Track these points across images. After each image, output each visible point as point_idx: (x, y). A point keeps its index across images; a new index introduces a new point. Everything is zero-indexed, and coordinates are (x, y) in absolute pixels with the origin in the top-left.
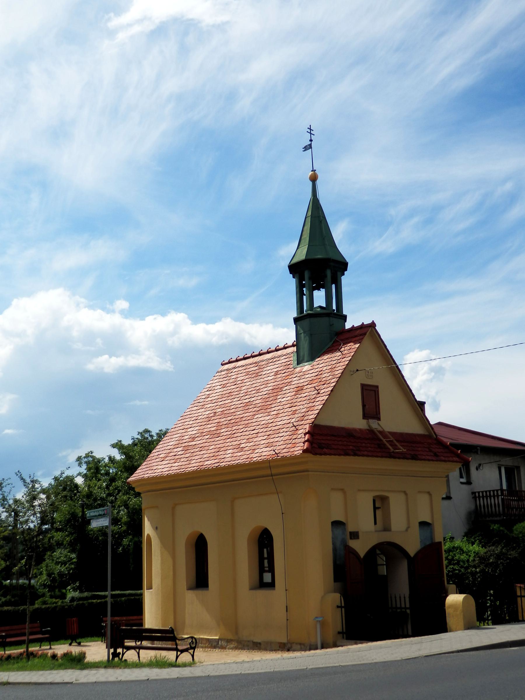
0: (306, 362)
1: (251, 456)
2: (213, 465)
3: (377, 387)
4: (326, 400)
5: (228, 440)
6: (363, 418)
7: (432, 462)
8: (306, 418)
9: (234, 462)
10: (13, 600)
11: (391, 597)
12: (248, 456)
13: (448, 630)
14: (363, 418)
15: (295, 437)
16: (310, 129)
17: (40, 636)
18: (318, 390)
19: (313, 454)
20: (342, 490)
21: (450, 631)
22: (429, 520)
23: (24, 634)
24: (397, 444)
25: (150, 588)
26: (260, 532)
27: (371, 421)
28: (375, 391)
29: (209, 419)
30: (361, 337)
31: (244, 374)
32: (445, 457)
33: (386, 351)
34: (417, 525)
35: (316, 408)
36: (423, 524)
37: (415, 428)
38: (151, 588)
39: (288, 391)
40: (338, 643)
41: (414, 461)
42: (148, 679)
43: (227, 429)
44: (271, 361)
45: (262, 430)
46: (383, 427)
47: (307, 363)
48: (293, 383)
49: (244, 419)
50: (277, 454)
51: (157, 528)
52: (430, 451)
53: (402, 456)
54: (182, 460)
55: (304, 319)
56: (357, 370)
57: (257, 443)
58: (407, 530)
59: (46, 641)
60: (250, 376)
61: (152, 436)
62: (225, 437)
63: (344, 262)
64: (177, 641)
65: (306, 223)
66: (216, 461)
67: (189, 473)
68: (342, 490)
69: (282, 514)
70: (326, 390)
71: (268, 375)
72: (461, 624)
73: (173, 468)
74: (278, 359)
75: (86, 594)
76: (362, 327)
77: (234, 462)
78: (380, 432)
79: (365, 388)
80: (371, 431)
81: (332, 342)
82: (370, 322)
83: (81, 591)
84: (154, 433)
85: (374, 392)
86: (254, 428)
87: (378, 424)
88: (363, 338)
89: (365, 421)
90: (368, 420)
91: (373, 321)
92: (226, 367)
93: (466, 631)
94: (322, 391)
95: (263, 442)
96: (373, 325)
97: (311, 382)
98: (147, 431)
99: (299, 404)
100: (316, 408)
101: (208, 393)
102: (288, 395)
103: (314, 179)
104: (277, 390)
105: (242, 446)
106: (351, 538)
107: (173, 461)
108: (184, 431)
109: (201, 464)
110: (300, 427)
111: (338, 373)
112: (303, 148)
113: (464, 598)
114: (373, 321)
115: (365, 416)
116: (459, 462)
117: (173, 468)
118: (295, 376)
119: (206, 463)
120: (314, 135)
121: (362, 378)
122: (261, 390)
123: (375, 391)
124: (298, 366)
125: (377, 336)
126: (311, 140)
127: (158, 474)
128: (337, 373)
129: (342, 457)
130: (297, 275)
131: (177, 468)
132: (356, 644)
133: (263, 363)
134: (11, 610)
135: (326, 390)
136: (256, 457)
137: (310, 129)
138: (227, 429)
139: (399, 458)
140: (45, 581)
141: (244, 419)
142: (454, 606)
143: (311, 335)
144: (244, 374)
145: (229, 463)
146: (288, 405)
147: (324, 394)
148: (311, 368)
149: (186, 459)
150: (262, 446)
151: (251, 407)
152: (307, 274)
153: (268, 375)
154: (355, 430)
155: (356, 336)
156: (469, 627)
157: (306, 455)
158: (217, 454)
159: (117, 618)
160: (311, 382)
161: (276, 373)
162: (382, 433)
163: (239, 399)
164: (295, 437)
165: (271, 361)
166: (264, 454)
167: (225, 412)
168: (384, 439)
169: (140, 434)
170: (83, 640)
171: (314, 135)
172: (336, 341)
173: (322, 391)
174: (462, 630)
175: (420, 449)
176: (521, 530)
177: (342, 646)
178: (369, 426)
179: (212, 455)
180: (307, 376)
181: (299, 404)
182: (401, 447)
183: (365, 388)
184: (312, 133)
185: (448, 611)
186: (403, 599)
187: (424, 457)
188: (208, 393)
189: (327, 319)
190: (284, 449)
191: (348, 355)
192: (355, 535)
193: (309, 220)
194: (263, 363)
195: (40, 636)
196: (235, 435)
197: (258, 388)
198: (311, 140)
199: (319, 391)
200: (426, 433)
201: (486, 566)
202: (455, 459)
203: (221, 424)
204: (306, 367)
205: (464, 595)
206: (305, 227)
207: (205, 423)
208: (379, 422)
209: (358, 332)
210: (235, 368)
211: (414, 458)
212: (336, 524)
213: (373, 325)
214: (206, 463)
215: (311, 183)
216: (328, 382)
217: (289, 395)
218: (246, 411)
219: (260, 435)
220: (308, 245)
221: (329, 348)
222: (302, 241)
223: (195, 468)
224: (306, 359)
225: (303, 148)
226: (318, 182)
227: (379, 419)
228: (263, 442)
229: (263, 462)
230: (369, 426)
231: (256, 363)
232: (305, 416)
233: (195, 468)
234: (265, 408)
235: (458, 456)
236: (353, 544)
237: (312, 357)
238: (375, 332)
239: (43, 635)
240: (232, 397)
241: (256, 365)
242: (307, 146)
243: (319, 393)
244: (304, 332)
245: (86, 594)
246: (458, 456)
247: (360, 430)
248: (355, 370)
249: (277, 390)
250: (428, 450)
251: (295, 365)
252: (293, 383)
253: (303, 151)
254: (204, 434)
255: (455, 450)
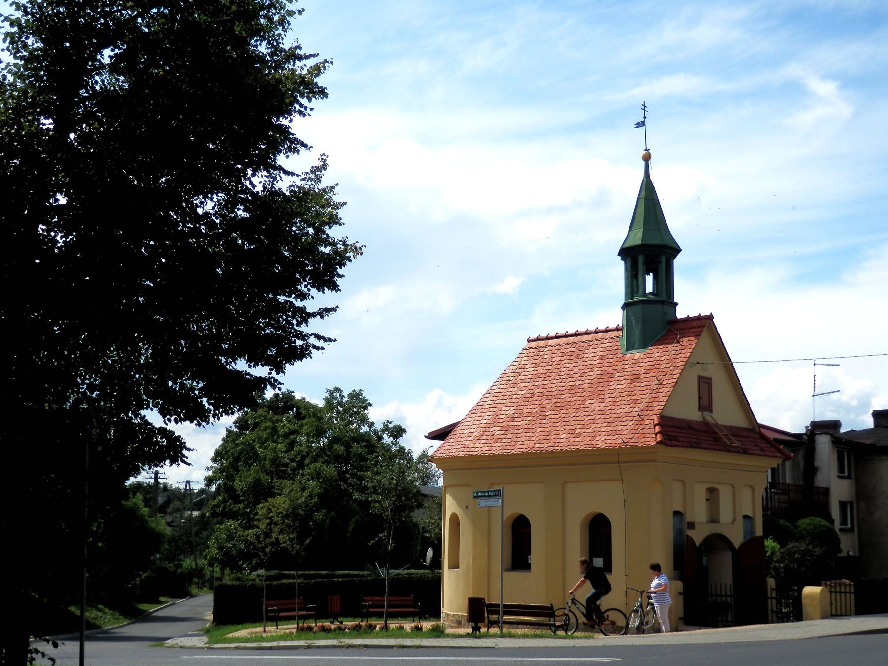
0: (638, 349)
1: (593, 442)
2: (547, 449)
3: (711, 379)
4: (671, 392)
5: (559, 424)
6: (699, 411)
7: (760, 457)
8: (651, 408)
9: (573, 447)
10: (153, 575)
11: (711, 586)
12: (589, 442)
13: (803, 619)
14: (699, 411)
15: (642, 427)
16: (644, 105)
17: (305, 613)
18: (659, 381)
19: (666, 446)
20: (682, 481)
21: (806, 620)
22: (750, 514)
23: (294, 610)
24: (732, 438)
25: (455, 565)
26: (517, 516)
27: (705, 413)
28: (709, 383)
29: (526, 399)
30: (700, 329)
31: (560, 355)
32: (770, 452)
33: (721, 344)
34: (742, 517)
35: (661, 399)
36: (746, 517)
37: (740, 422)
38: (458, 567)
39: (622, 379)
40: (679, 629)
41: (746, 455)
42: (574, 646)
43: (553, 413)
44: (591, 343)
45: (599, 417)
46: (716, 419)
47: (638, 351)
48: (626, 370)
49: (573, 403)
50: (625, 443)
51: (467, 507)
52: (757, 446)
53: (737, 451)
54: (505, 440)
55: (636, 305)
56: (698, 363)
57: (597, 430)
58: (733, 522)
59: (312, 618)
60: (568, 358)
61: (343, 397)
62: (554, 420)
63: (678, 248)
64: (556, 617)
65: (639, 203)
66: (549, 444)
67: (517, 454)
68: (682, 481)
69: (624, 501)
70: (670, 381)
71: (592, 358)
72: (818, 613)
73: (494, 449)
74: (600, 342)
75: (273, 572)
76: (699, 318)
77: (573, 447)
78: (714, 425)
79: (700, 378)
80: (706, 423)
81: (666, 331)
82: (709, 314)
83: (268, 569)
84: (346, 393)
85: (708, 385)
86: (588, 414)
87: (712, 417)
88: (702, 331)
89: (700, 413)
90: (702, 412)
91: (711, 313)
92: (534, 344)
93: (826, 621)
94: (665, 382)
95: (604, 429)
96: (710, 317)
97: (648, 371)
98: (338, 390)
99: (638, 393)
100: (661, 399)
101: (517, 371)
102: (620, 384)
103: (647, 158)
104: (607, 376)
105: (577, 431)
106: (688, 529)
107: (493, 441)
108: (496, 409)
109: (531, 446)
110: (646, 418)
111: (680, 364)
112: (635, 125)
113: (822, 590)
114: (711, 313)
115: (701, 408)
116: (781, 458)
117: (494, 449)
118: (626, 362)
119: (537, 446)
120: (647, 111)
121: (698, 371)
122: (586, 374)
123: (709, 383)
124: (627, 352)
125: (714, 328)
126: (645, 118)
127: (476, 453)
128: (678, 364)
129: (689, 449)
130: (629, 260)
131: (500, 448)
132: (700, 629)
133: (582, 345)
134: (236, 585)
135: (670, 381)
136: (598, 444)
137: (644, 105)
138: (553, 413)
139: (734, 452)
140: (216, 555)
141: (573, 403)
142: (811, 596)
143: (644, 322)
144: (560, 355)
145: (567, 448)
146: (625, 394)
147: (667, 385)
148: (645, 356)
149: (509, 440)
150: (604, 434)
151: (578, 391)
152: (641, 259)
153: (592, 358)
154: (691, 422)
155: (694, 327)
156: (675, 629)
157: (659, 446)
158: (548, 437)
159: (377, 598)
160: (648, 371)
161: (602, 358)
162: (717, 425)
163: (560, 381)
164: (642, 427)
165: (591, 343)
166: (609, 442)
167: (546, 394)
168: (721, 432)
169: (328, 393)
170: (345, 619)
171: (647, 111)
172: (669, 330)
173: (665, 382)
174: (819, 619)
175: (748, 443)
176: (804, 527)
177: (686, 631)
178: (703, 418)
179: (542, 438)
180: (642, 364)
181: (638, 393)
182: (736, 442)
183: (700, 378)
184: (643, 106)
185: (804, 601)
186: (723, 588)
187: (753, 452)
188: (517, 371)
189: (659, 306)
190: (632, 438)
191: (688, 347)
192: (691, 526)
193: (643, 202)
194: (582, 345)
195: (305, 613)
196: (567, 419)
197: (582, 371)
198: (645, 118)
199: (661, 381)
200: (751, 427)
201: (791, 562)
202: (779, 455)
203: (544, 406)
204: (638, 354)
205: (821, 587)
206: (638, 210)
207: (523, 403)
208: (711, 414)
209: (695, 323)
210: (546, 346)
211: (745, 452)
212: (677, 513)
213: (710, 317)
214: (537, 446)
215: (643, 163)
216: (669, 373)
217: (623, 382)
218: (574, 395)
219: (597, 421)
220: (642, 229)
221: (662, 337)
222: (635, 224)
223: (524, 450)
224: (637, 346)
225: (635, 125)
226: (652, 163)
227: (711, 411)
228: (604, 429)
229: (609, 450)
230: (704, 418)
231: (572, 343)
232: (650, 407)
233: (524, 450)
234: (596, 393)
235: (780, 451)
236: (690, 533)
237: (644, 345)
238: (712, 324)
239: (307, 611)
240: (551, 378)
241: (574, 346)
242: (639, 123)
243: (661, 384)
244: (636, 319)
245: (273, 572)
246: (780, 451)
247: (697, 422)
248: (696, 362)
249: (607, 376)
250: (754, 444)
251: (623, 351)
252: (626, 370)
253: (636, 128)
254: (525, 415)
255: (778, 445)
